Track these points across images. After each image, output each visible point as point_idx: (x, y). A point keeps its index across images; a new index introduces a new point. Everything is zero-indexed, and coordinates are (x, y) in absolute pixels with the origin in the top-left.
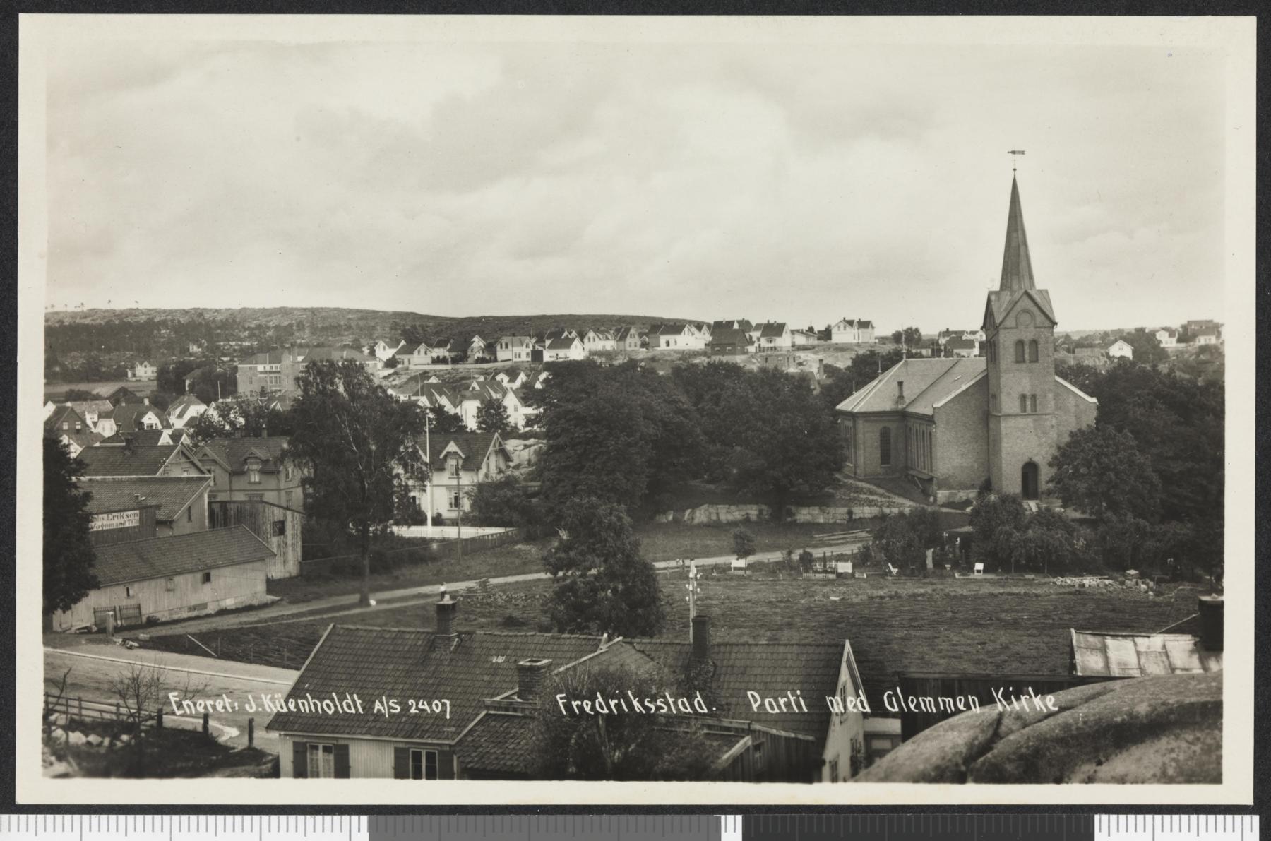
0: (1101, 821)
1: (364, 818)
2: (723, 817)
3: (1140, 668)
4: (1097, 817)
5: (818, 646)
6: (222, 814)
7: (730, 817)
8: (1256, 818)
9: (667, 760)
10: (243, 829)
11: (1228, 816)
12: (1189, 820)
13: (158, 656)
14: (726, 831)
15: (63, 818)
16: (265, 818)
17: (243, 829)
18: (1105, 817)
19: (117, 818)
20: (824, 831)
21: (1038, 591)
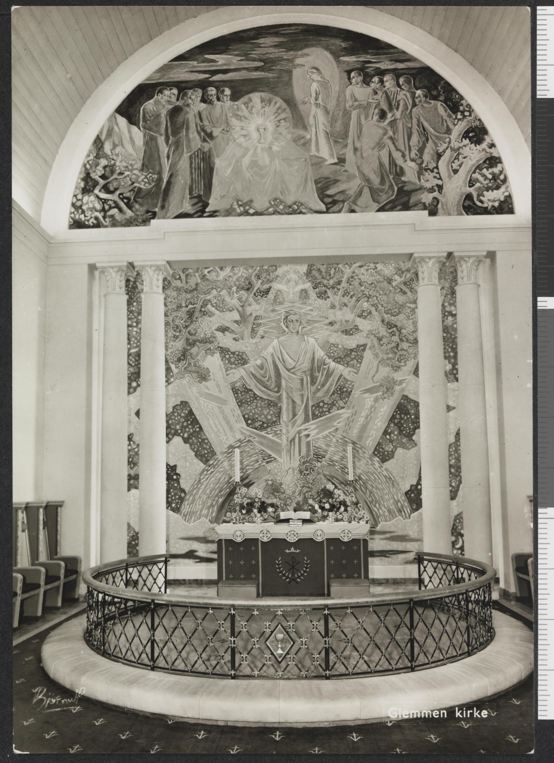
0: (540, 95)
1: (540, 510)
2: (538, 308)
3: (420, 189)
4: (538, 97)
6: (536, 46)
7: (539, 304)
8: (538, 8)
9: (504, 212)
13: (217, 184)
16: (538, 88)
18: (538, 93)
21: (189, 392)
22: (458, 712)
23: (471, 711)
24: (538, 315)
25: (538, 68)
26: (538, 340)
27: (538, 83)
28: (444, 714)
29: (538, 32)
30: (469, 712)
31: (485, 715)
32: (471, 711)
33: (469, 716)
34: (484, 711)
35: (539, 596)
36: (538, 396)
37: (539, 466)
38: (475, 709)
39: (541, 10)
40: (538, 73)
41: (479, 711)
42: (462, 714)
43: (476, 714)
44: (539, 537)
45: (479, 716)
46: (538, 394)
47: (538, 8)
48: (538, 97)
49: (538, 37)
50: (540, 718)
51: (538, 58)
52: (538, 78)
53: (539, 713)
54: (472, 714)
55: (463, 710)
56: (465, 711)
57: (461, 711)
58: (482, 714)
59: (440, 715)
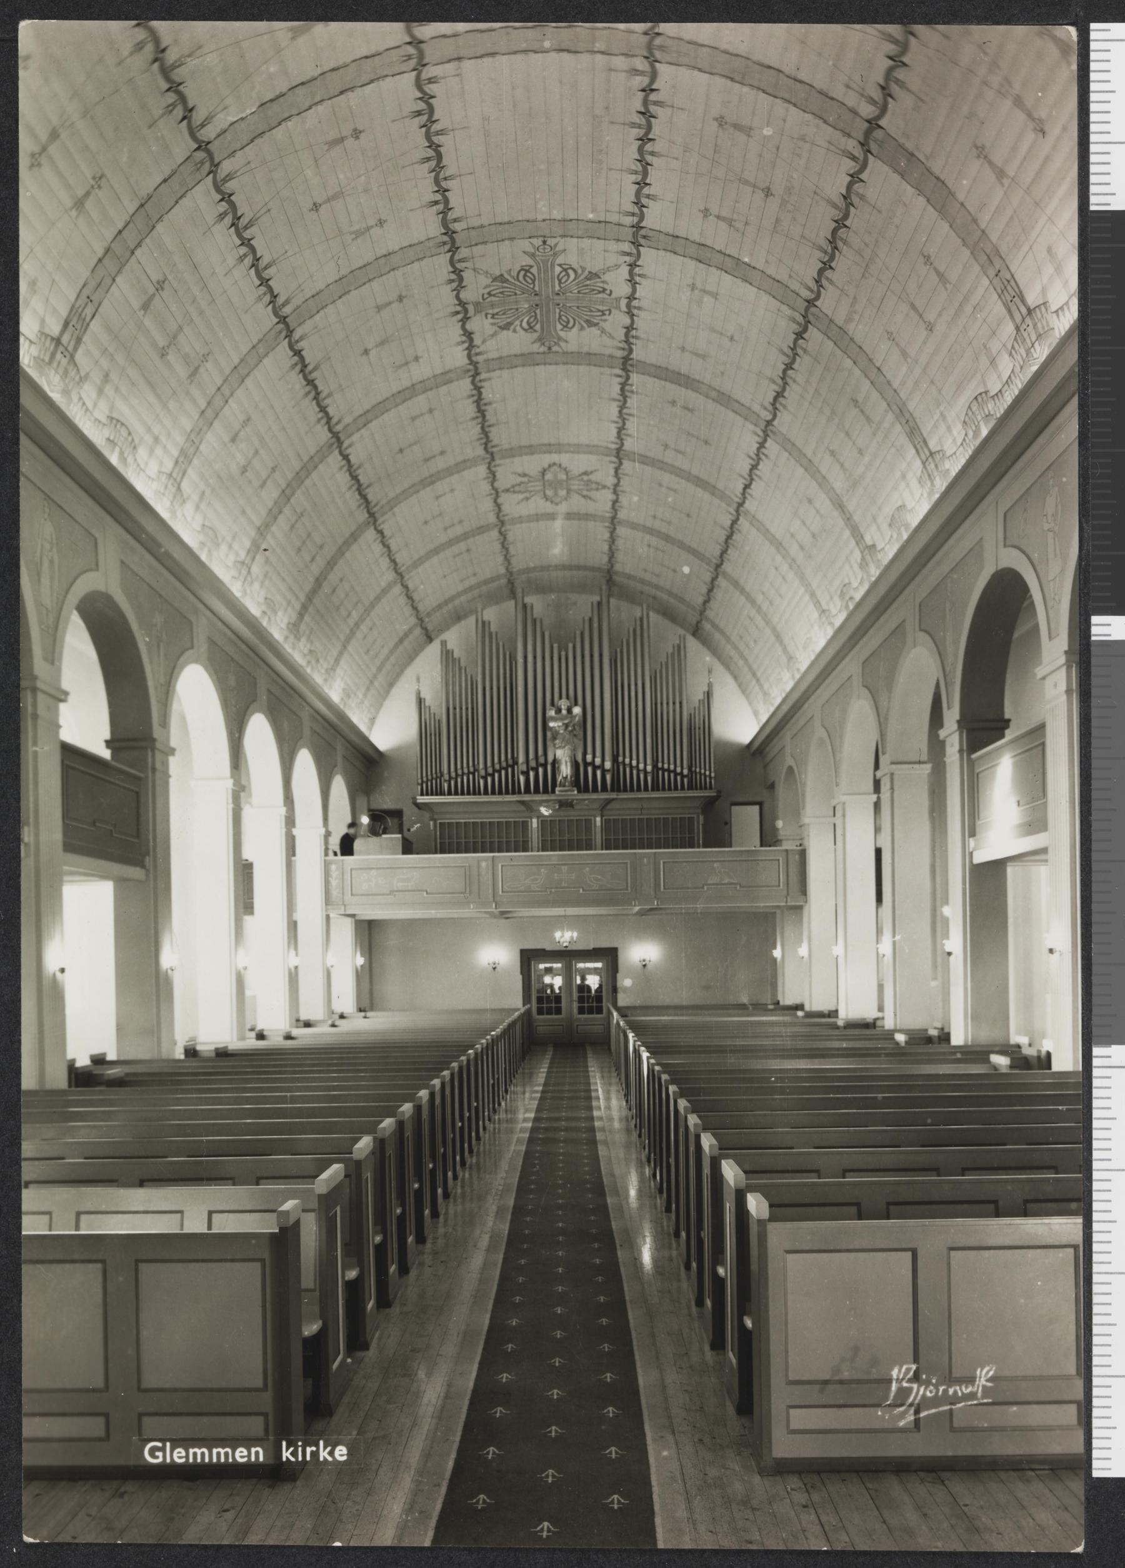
0: (1096, 203)
1: (1096, 1051)
2: (1093, 638)
4: (1092, 208)
5: (813, 595)
8: (1093, 26)
10: (1108, 1418)
11: (1092, 37)
12: (1099, 1222)
14: (1110, 635)
15: (1096, 1294)
16: (1093, 189)
17: (1108, 1418)
18: (1093, 199)
19: (1095, 1067)
20: (1109, 327)
22: (287, 1450)
23: (314, 1449)
24: (1093, 653)
25: (1093, 148)
26: (1093, 704)
27: (1093, 179)
28: (257, 1453)
29: (1093, 76)
30: (309, 1450)
31: (342, 1455)
32: (314, 1449)
33: (308, 1458)
34: (241, 1449)
35: (1094, 1225)
36: (1093, 817)
37: (1094, 961)
38: (321, 1443)
39: (1099, 31)
40: (1093, 158)
41: (329, 1449)
42: (294, 1454)
43: (324, 1454)
44: (1094, 1105)
45: (330, 1459)
46: (1093, 813)
47: (1093, 26)
48: (1092, 208)
49: (1093, 87)
50: (1096, 1474)
51: (1093, 128)
52: (1093, 169)
53: (1095, 1464)
54: (315, 1455)
55: (296, 1447)
56: (300, 1449)
57: (292, 1449)
58: (337, 1453)
59: (187, 1457)
